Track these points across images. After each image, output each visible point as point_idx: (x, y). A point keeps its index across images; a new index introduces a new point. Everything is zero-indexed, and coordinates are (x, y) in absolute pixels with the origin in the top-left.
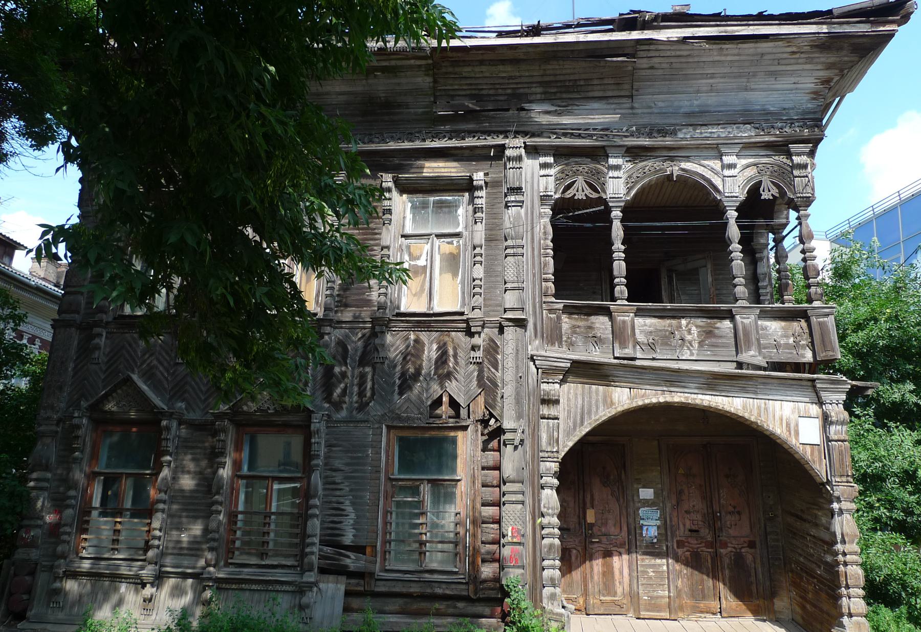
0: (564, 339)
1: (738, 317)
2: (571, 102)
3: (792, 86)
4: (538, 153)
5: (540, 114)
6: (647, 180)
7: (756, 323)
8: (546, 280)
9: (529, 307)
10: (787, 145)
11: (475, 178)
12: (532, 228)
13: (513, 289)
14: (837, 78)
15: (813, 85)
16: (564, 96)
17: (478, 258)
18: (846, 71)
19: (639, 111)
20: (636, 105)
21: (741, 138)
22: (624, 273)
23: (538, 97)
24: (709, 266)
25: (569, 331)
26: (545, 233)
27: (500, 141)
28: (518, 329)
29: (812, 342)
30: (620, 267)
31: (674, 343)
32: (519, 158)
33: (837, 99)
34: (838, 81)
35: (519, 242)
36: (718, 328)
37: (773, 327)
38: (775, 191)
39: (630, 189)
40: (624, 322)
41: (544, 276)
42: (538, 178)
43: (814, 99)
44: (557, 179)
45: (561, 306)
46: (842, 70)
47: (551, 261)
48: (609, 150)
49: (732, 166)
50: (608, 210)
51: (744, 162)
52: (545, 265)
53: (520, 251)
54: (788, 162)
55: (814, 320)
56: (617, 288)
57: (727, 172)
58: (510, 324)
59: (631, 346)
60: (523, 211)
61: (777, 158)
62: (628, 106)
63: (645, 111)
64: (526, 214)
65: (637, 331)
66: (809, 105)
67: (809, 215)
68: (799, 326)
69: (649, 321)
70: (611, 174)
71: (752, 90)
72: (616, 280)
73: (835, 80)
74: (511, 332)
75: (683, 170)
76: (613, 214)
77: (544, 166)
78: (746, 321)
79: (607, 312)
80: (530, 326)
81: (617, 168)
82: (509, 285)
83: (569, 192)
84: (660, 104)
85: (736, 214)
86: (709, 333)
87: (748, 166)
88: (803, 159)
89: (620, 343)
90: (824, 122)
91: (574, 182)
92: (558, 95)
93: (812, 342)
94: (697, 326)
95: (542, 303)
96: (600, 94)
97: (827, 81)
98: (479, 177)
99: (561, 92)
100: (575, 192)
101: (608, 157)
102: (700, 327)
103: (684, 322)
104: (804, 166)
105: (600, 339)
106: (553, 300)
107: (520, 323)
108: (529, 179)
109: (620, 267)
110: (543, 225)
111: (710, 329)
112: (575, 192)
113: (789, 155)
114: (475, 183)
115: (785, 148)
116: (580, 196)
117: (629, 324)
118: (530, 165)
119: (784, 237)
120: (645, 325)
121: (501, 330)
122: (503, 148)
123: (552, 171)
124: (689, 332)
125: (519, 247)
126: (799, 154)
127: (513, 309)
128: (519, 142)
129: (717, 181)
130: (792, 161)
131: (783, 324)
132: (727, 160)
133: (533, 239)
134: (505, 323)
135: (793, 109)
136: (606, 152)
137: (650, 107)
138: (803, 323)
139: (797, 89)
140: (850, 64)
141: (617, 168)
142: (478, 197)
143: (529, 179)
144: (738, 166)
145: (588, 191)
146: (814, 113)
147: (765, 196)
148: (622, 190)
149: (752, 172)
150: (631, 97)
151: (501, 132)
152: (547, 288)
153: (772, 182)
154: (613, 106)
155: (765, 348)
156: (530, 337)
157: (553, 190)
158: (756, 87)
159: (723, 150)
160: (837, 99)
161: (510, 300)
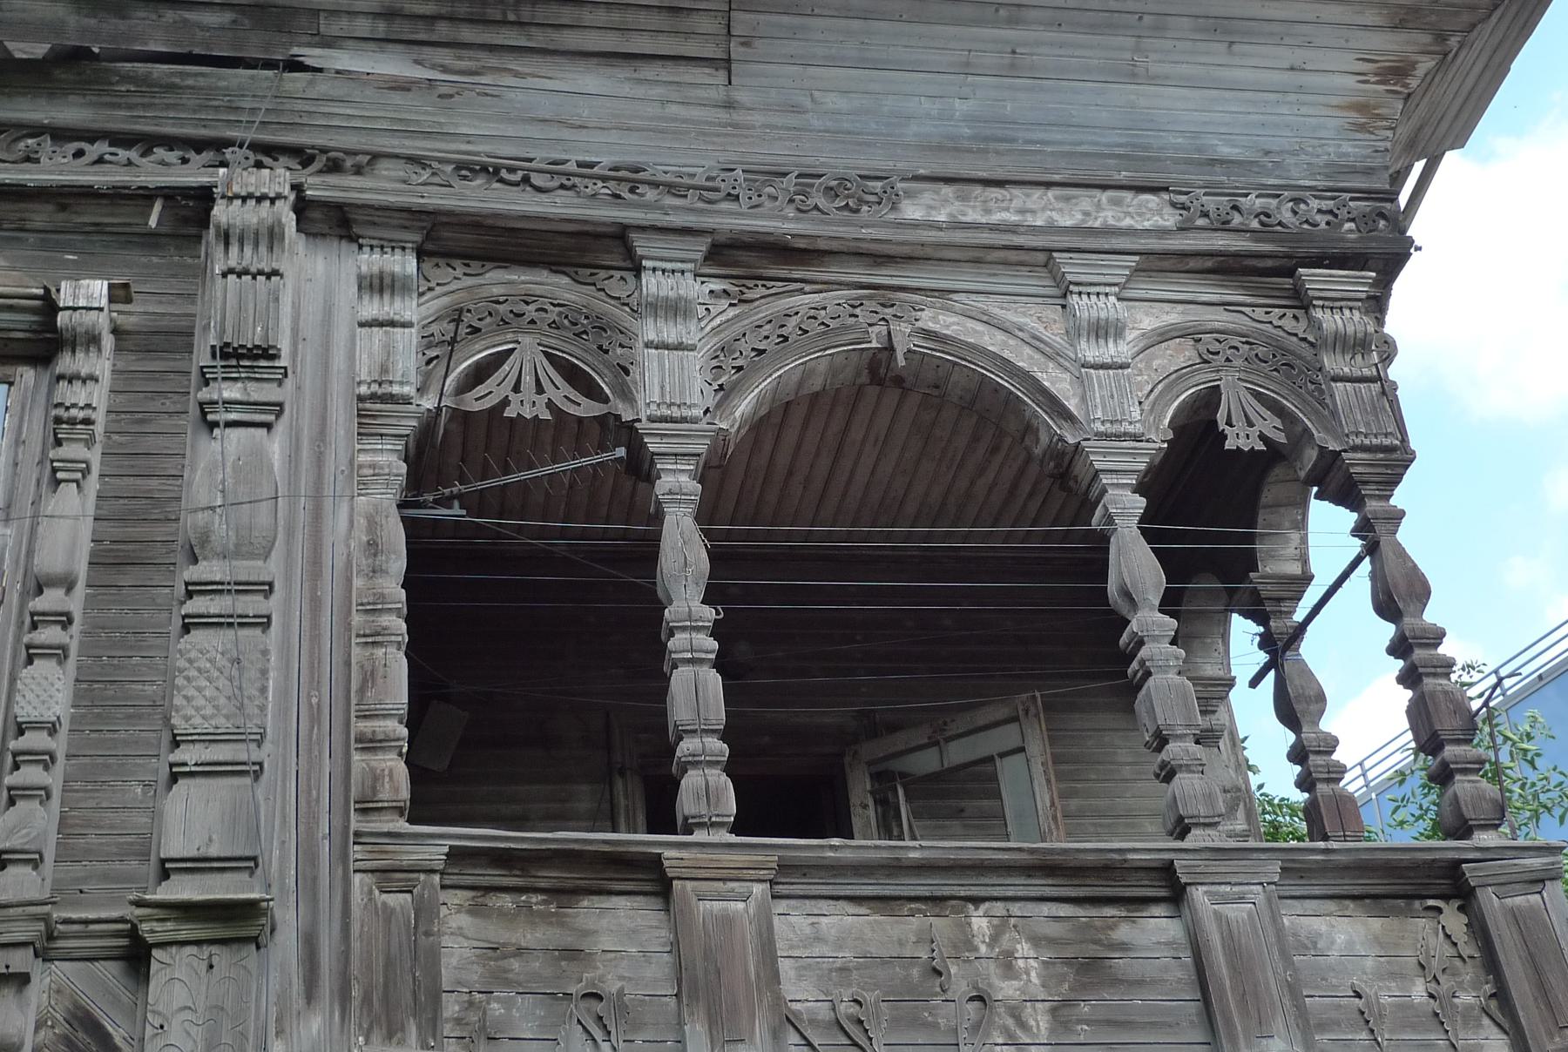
0: (451, 1007)
1: (1199, 894)
2: (493, 61)
3: (1287, 76)
4: (353, 239)
5: (360, 83)
6: (790, 366)
7: (1275, 918)
8: (371, 744)
9: (280, 859)
10: (1290, 273)
11: (65, 298)
12: (317, 515)
13: (210, 771)
14: (1426, 64)
15: (1351, 81)
16: (468, 34)
17: (49, 634)
18: (1453, 42)
19: (757, 118)
20: (741, 96)
21: (1131, 232)
22: (717, 713)
23: (362, 27)
24: (1037, 748)
25: (475, 975)
26: (373, 547)
27: (193, 174)
28: (221, 955)
29: (1501, 995)
30: (696, 692)
31: (945, 1016)
32: (273, 236)
33: (1419, 166)
34: (1430, 76)
35: (247, 569)
36: (1123, 946)
37: (1341, 938)
38: (1270, 425)
39: (726, 393)
40: (727, 921)
41: (366, 726)
42: (350, 333)
43: (1361, 128)
44: (428, 341)
45: (435, 853)
46: (1441, 38)
47: (398, 668)
48: (642, 245)
49: (1102, 330)
50: (640, 467)
51: (1148, 320)
52: (369, 677)
53: (251, 605)
54: (1300, 328)
55: (1489, 900)
56: (691, 781)
57: (1091, 351)
58: (187, 931)
59: (761, 1030)
60: (275, 446)
61: (1259, 313)
62: (718, 94)
63: (779, 120)
64: (293, 459)
65: (785, 966)
66: (1347, 148)
67: (1401, 515)
68: (1435, 931)
69: (838, 921)
70: (650, 330)
71: (1153, 80)
72: (687, 746)
73: (1421, 70)
74: (178, 977)
75: (928, 334)
76: (664, 484)
77: (378, 285)
78: (1237, 912)
79: (654, 880)
80: (286, 942)
81: (675, 309)
82: (189, 755)
83: (481, 390)
84: (833, 101)
85: (1141, 502)
86: (1089, 969)
87: (1164, 336)
88: (1351, 321)
89: (713, 1022)
90: (1403, 199)
91: (499, 359)
92: (443, 31)
93: (1501, 995)
94: (1036, 941)
95: (346, 838)
96: (610, 42)
97: (1397, 72)
98: (86, 295)
99: (451, 19)
100: (506, 390)
101: (638, 270)
102: (1052, 942)
103: (980, 923)
104: (1360, 345)
105: (621, 1006)
106: (402, 825)
107: (235, 923)
108: (310, 326)
109: (696, 692)
110: (362, 525)
111: (1093, 950)
112: (506, 390)
113: (1301, 301)
114: (62, 319)
115: (1287, 282)
116: (527, 406)
117: (749, 932)
118: (319, 275)
119: (1302, 628)
120: (818, 939)
121: (136, 956)
122: (205, 196)
123: (408, 308)
124: (1007, 964)
125: (244, 588)
126: (1335, 303)
127: (199, 865)
128: (278, 178)
129: (1058, 382)
130: (1315, 325)
131: (1376, 924)
132: (1085, 307)
133: (316, 561)
134: (152, 930)
135: (1294, 153)
136: (629, 253)
137: (796, 109)
138: (1454, 921)
139: (1300, 90)
140: (1466, 18)
141: (675, 309)
142: (71, 379)
143: (310, 326)
144: (1130, 335)
145: (560, 391)
146: (1369, 172)
147: (1239, 439)
148: (697, 393)
149: (1178, 355)
150: (726, 63)
151: (199, 145)
152: (375, 778)
153: (1258, 396)
154: (657, 91)
155: (1322, 1027)
156: (283, 999)
157: (413, 377)
158: (1166, 68)
159: (1072, 268)
160: (1419, 166)
161: (191, 820)
